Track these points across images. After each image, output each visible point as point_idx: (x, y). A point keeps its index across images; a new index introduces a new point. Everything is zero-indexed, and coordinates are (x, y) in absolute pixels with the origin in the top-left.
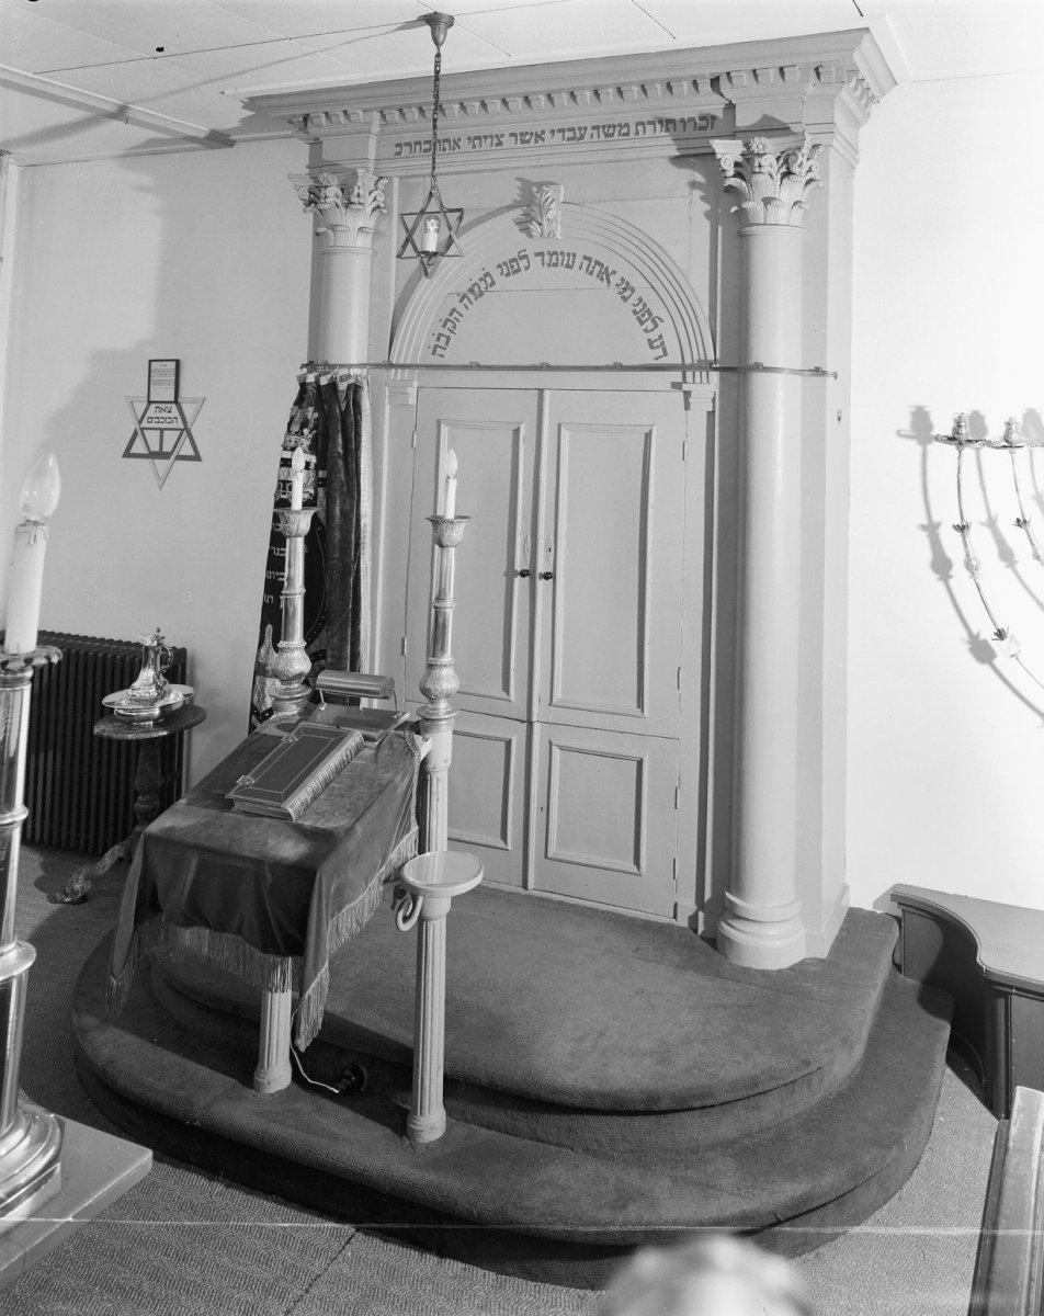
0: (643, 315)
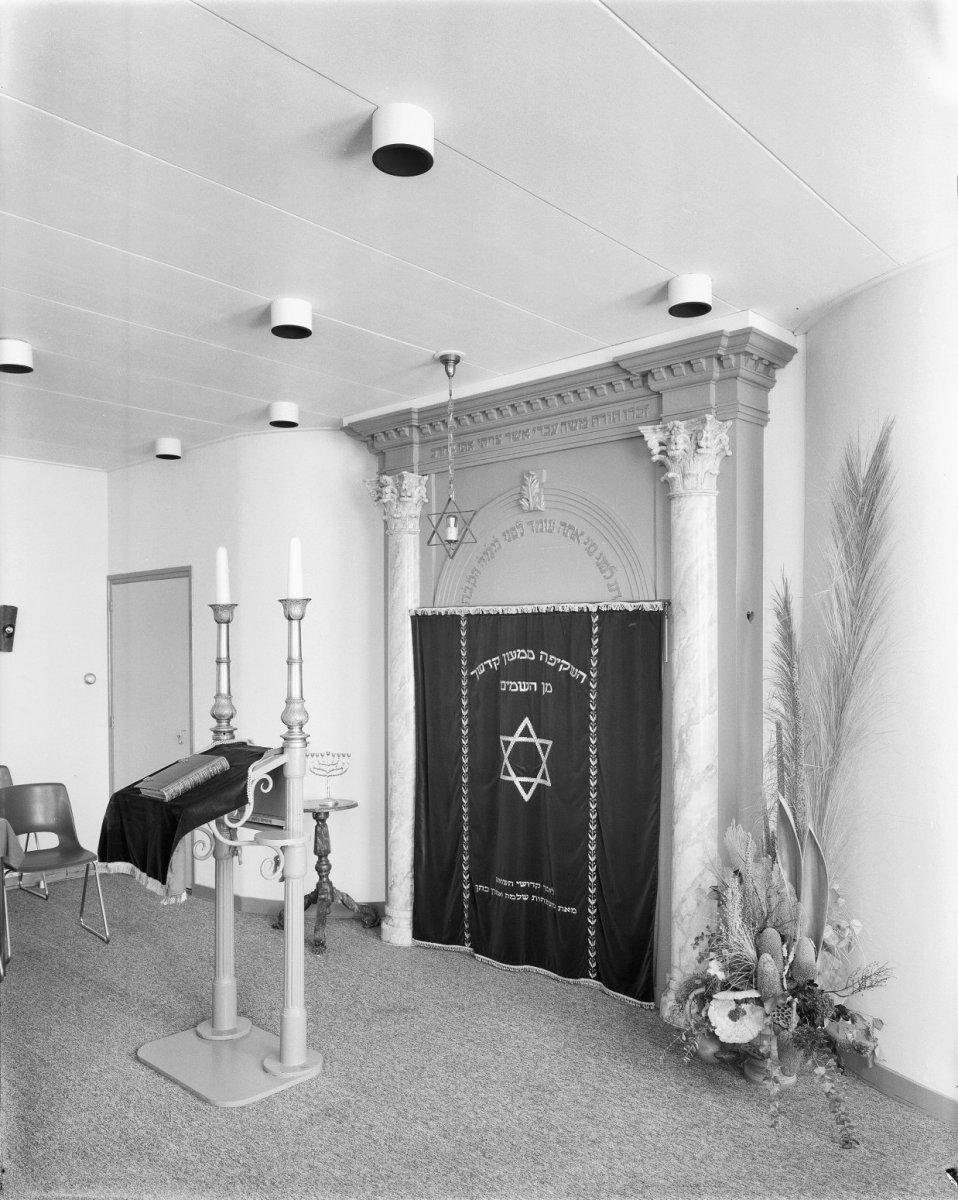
0: (603, 565)
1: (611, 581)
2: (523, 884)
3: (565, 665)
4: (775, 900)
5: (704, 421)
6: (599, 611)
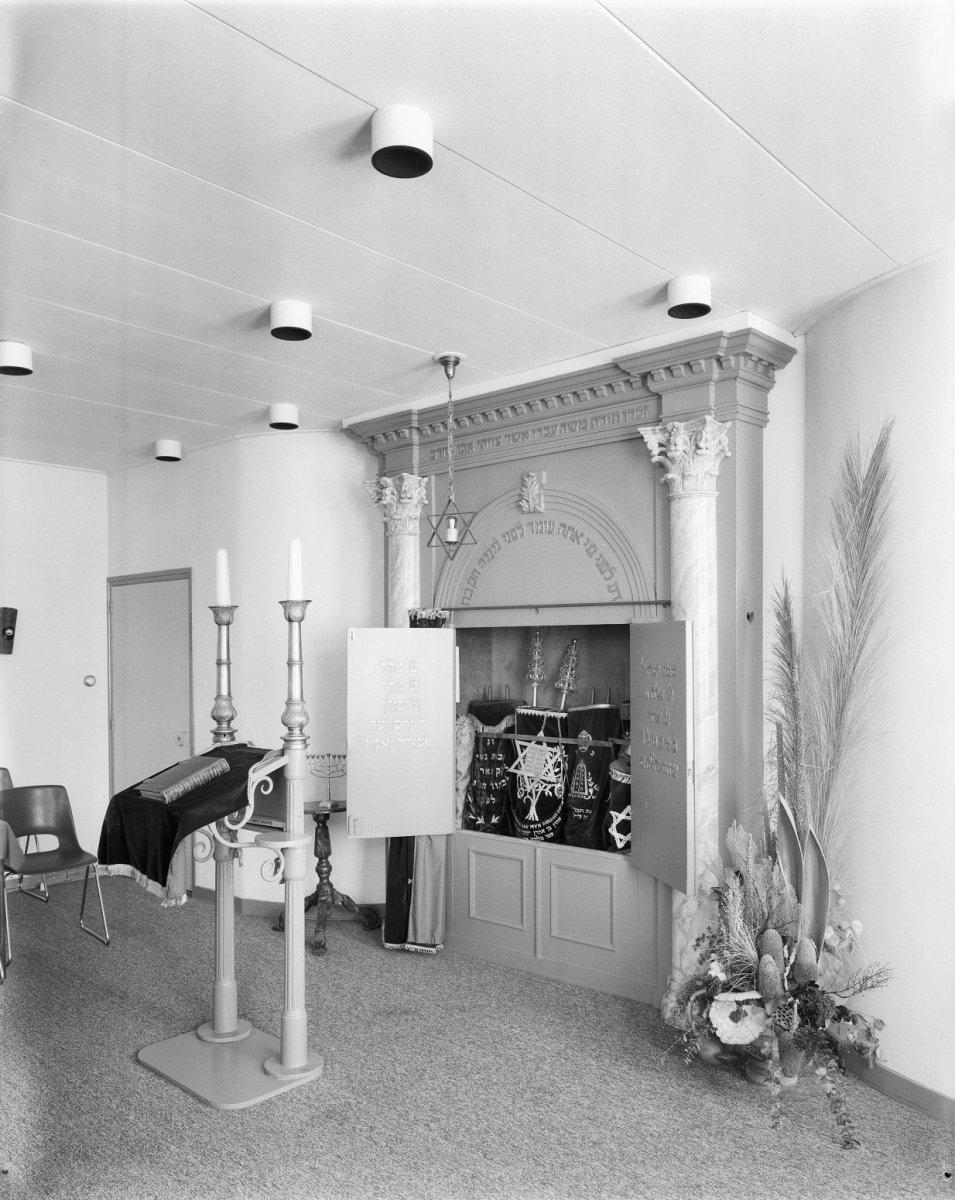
0: (603, 566)
1: (611, 582)
4: (775, 901)
5: (704, 422)
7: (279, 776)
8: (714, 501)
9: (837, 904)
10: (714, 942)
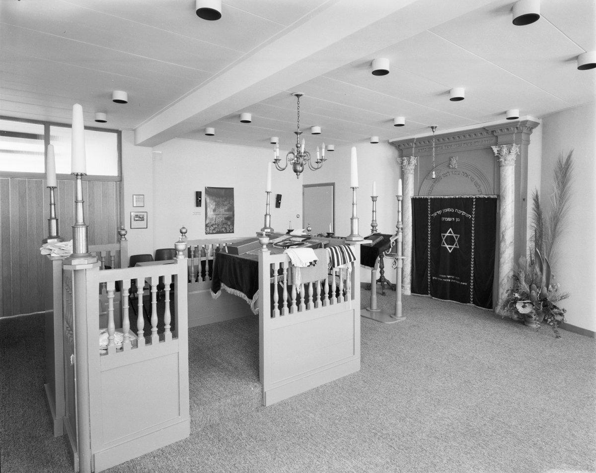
0: (476, 184)
2: (449, 277)
3: (464, 213)
4: (534, 277)
5: (512, 145)
6: (476, 198)
7: (396, 241)
8: (514, 167)
9: (553, 278)
10: (515, 289)
